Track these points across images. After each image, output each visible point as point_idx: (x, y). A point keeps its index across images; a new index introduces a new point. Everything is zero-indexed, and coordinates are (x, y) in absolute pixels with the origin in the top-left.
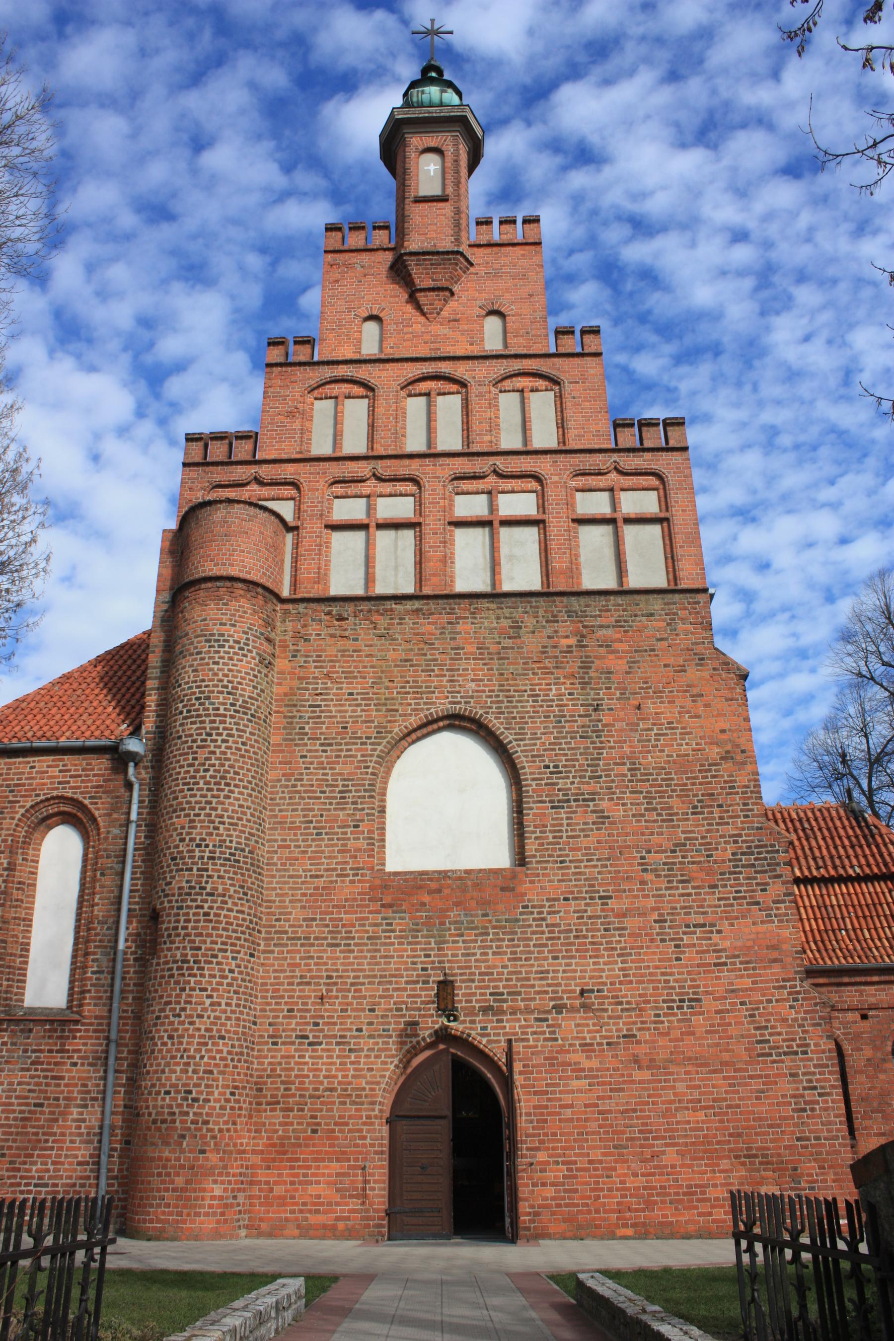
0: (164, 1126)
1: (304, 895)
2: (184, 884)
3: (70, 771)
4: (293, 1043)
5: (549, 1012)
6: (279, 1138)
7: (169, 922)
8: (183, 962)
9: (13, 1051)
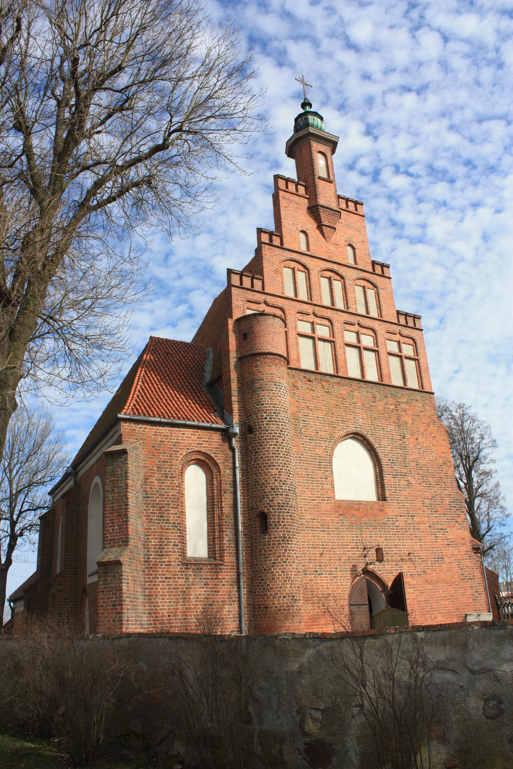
0: (285, 612)
1: (309, 508)
2: (280, 501)
3: (202, 438)
4: (312, 574)
5: (399, 561)
6: (312, 616)
7: (275, 519)
8: (284, 537)
9: (195, 579)
